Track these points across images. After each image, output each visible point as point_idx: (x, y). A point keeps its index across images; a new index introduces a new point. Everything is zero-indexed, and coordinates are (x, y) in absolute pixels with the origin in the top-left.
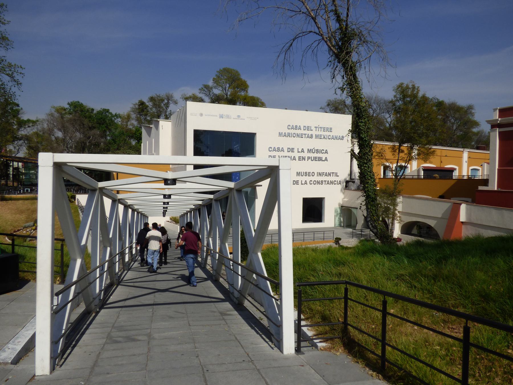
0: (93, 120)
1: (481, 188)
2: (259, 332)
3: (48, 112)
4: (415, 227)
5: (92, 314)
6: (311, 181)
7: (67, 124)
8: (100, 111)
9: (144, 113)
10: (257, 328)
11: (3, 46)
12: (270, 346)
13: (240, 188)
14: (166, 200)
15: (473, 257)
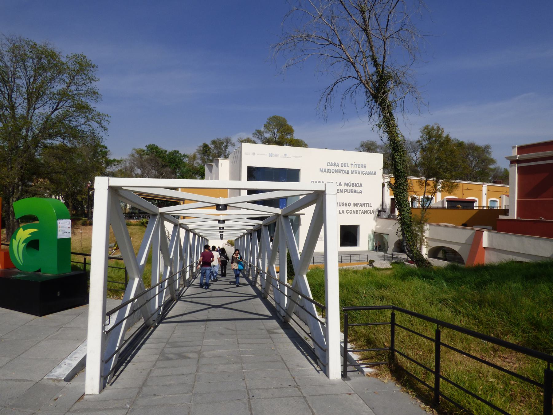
0: (166, 160)
1: (501, 217)
2: (305, 352)
3: (130, 153)
4: (441, 252)
5: (151, 328)
6: (348, 210)
7: (145, 163)
8: (171, 152)
9: (207, 154)
10: (303, 348)
11: (93, 99)
12: (316, 369)
13: (286, 214)
14: (221, 225)
15: (514, 283)
